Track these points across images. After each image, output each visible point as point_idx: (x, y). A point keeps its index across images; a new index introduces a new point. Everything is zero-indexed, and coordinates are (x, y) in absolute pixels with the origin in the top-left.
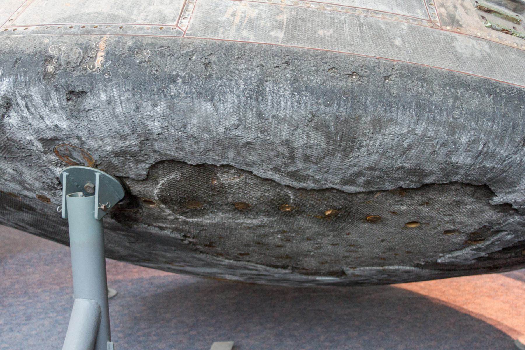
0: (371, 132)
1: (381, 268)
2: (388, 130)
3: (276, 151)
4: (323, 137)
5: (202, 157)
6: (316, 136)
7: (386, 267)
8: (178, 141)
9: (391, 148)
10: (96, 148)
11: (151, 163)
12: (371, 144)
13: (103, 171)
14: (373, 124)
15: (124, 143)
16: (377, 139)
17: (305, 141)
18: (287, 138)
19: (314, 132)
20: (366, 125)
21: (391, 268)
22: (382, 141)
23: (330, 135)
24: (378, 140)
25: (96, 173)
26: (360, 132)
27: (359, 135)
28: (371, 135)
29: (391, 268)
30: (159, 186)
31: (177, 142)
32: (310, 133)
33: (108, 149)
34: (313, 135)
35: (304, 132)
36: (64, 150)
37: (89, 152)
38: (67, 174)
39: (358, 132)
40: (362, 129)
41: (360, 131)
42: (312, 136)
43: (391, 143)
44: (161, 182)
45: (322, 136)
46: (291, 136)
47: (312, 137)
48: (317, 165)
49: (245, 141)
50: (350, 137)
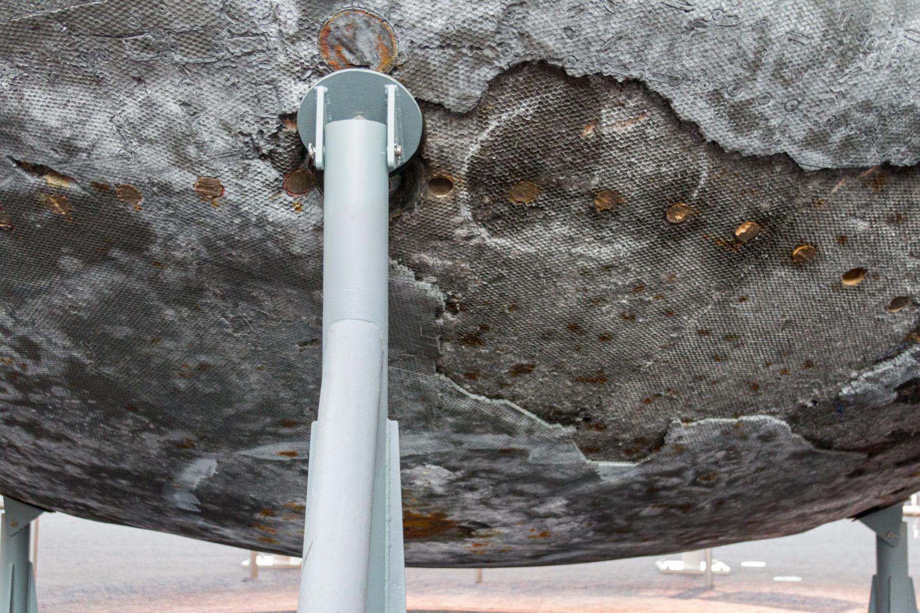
0: (891, 21)
1: (735, 421)
2: (914, 22)
3: (738, 44)
4: (821, 21)
5: (602, 54)
6: (811, 16)
7: (744, 418)
8: (577, 10)
9: (911, 61)
10: (413, 22)
11: (501, 68)
12: (886, 47)
13: (402, 82)
14: (895, 6)
15: (474, 9)
16: (897, 37)
17: (792, 26)
18: (766, 14)
19: (811, 8)
20: (886, 7)
21: (753, 418)
22: (903, 42)
23: (832, 18)
24: (898, 40)
25: (387, 86)
26: (876, 19)
27: (874, 24)
28: (889, 28)
29: (753, 418)
30: (484, 136)
31: (573, 13)
32: (804, 9)
33: (435, 25)
34: (807, 13)
35: (795, 7)
36: (347, 25)
37: (397, 31)
38: (326, 89)
39: (873, 19)
40: (879, 14)
41: (877, 17)
42: (806, 16)
43: (914, 48)
44: (493, 124)
45: (822, 17)
46: (773, 12)
47: (805, 18)
48: (786, 89)
49: (696, 16)
50: (860, 25)
